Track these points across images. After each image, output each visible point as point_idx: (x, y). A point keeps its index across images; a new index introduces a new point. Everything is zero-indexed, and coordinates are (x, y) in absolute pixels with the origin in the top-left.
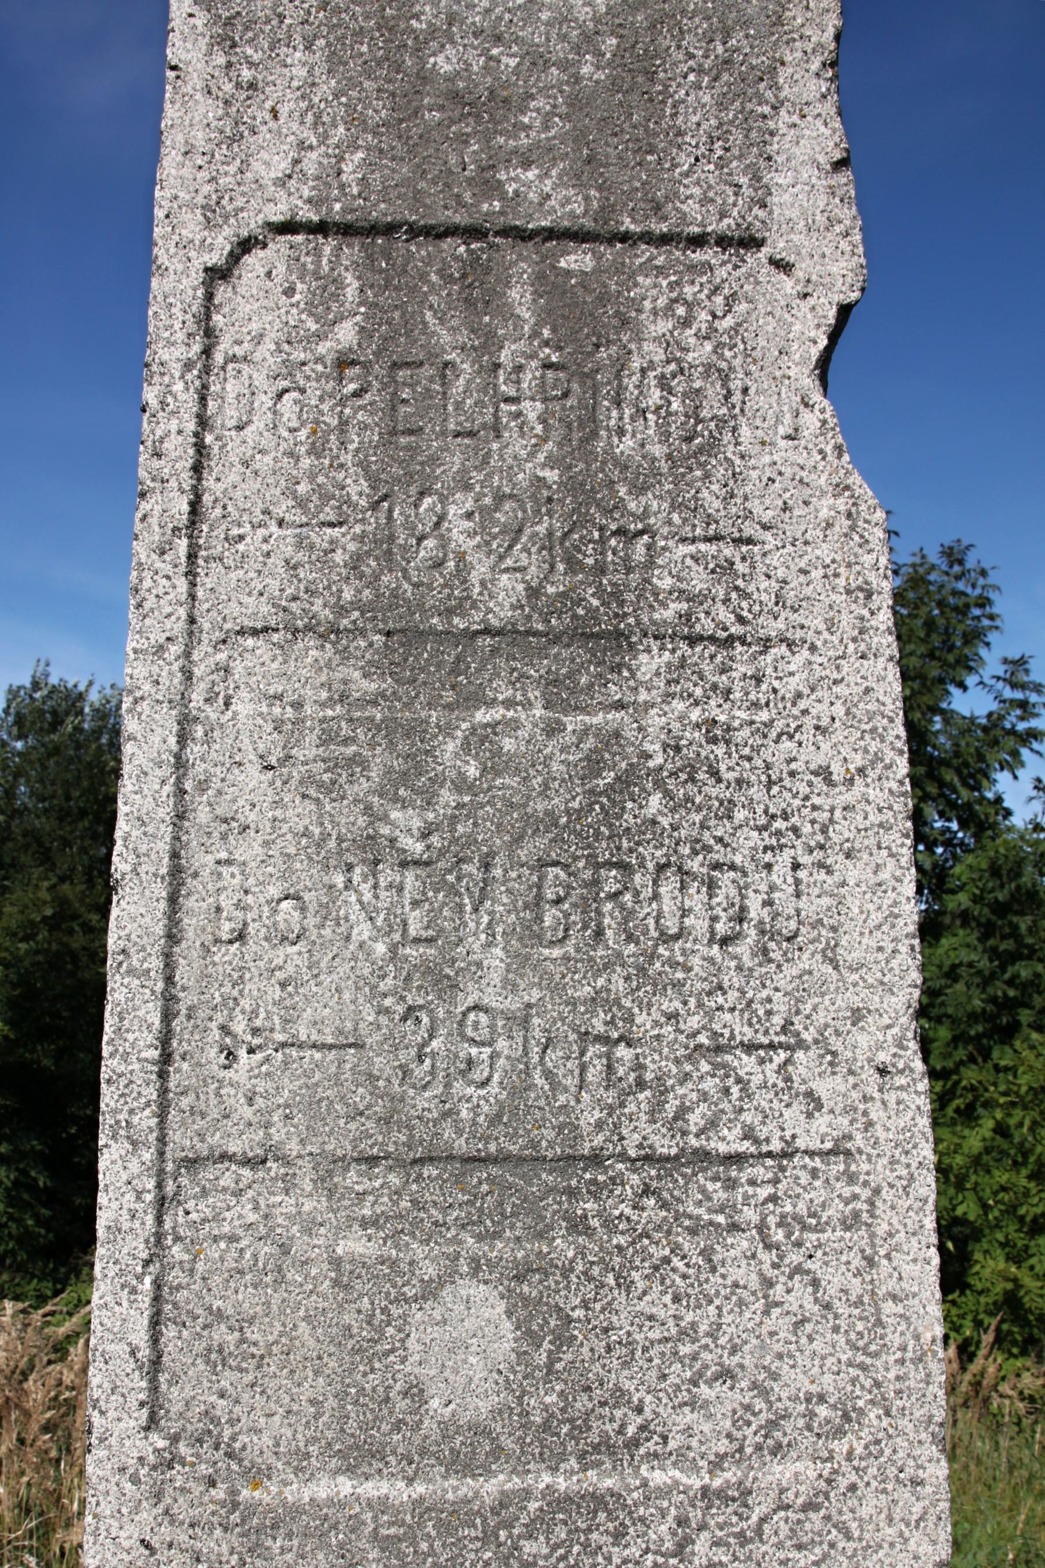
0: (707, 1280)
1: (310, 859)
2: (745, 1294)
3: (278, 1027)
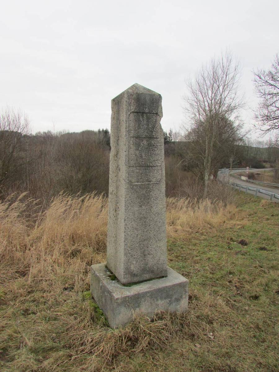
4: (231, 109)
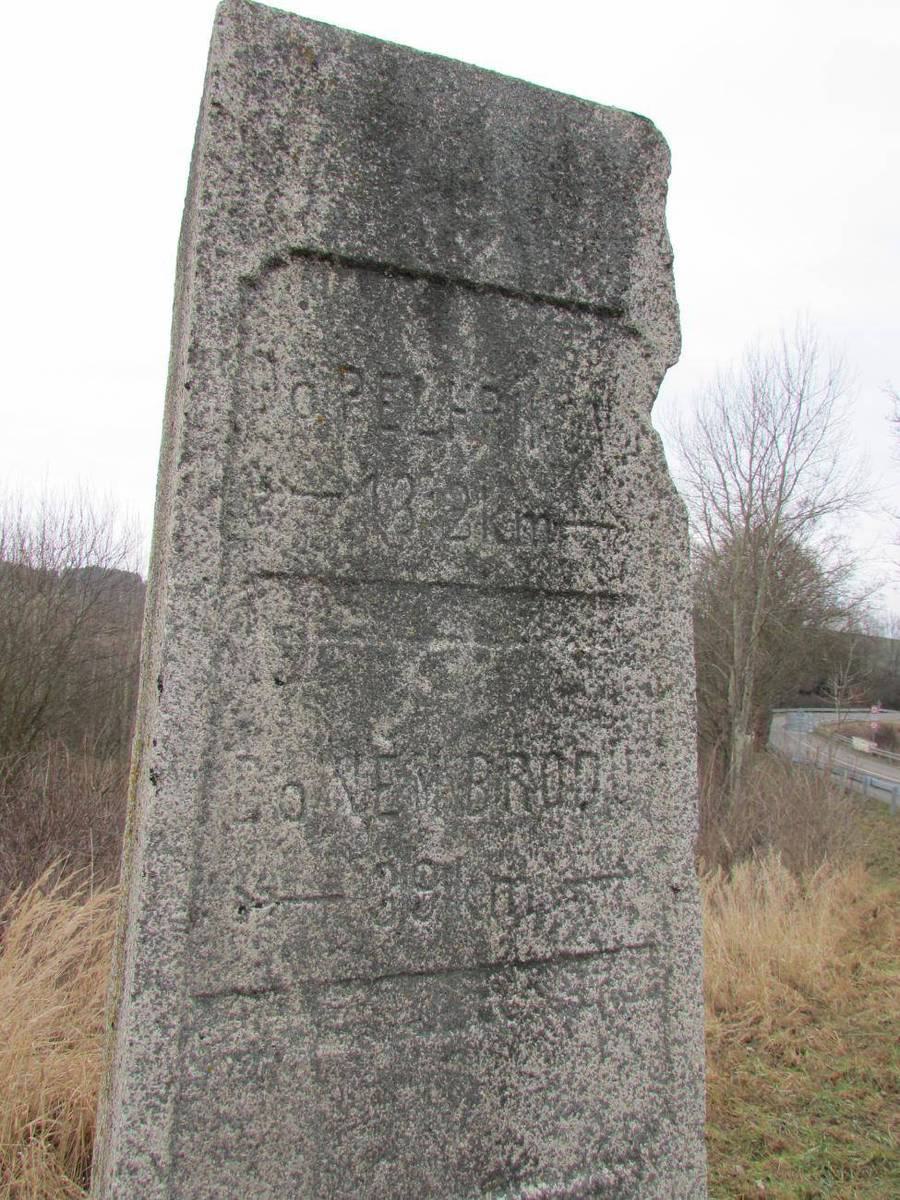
0: (567, 1044)
1: (309, 754)
2: (589, 1050)
3: (280, 885)
4: (812, 513)
